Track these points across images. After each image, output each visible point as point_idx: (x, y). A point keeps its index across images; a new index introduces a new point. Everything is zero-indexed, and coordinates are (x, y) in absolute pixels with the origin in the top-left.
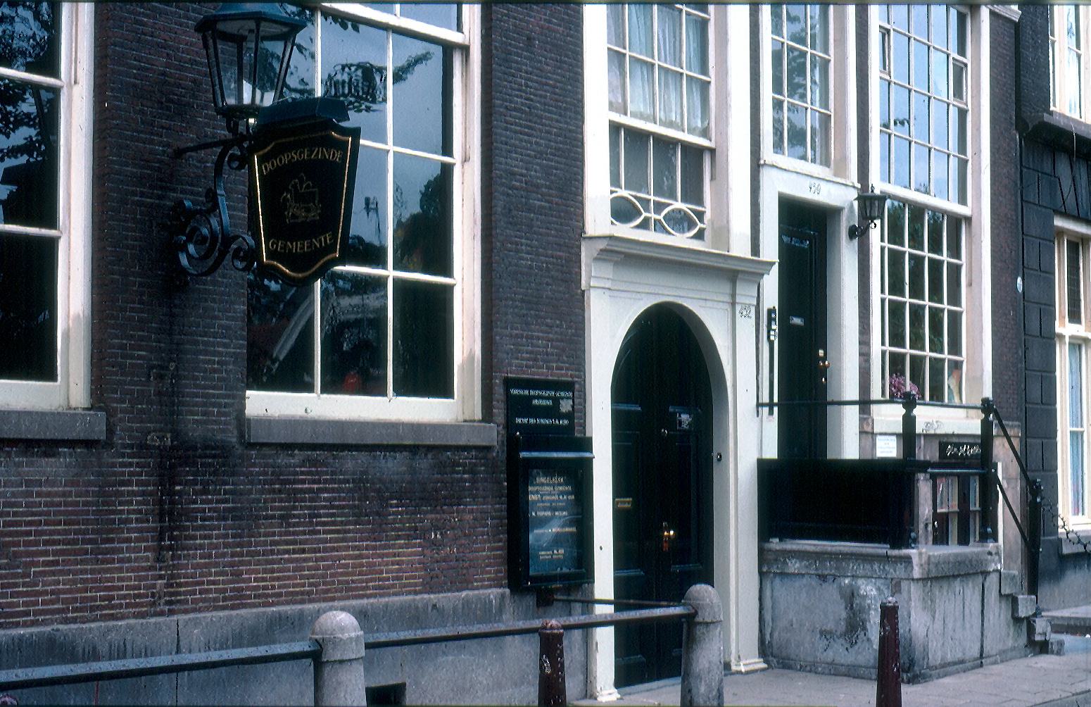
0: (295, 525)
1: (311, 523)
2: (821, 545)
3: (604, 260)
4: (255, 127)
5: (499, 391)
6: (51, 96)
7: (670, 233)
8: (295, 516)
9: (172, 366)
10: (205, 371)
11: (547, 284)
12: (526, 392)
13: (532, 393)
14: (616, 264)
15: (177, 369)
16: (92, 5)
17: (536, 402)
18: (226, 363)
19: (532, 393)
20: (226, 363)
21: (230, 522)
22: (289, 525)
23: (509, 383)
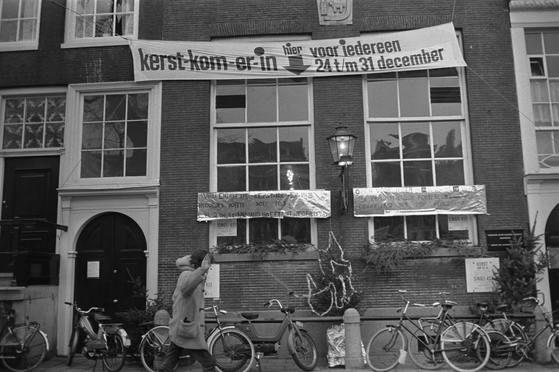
0: (390, 283)
1: (397, 283)
2: (36, 28)
3: (529, 183)
4: (135, 353)
5: (484, 237)
6: (459, 154)
7: (548, 167)
8: (390, 280)
9: (341, 237)
10: (353, 238)
11: (506, 195)
12: (496, 235)
13: (499, 235)
14: (541, 183)
15: (343, 238)
16: (36, 48)
17: (501, 238)
18: (361, 235)
19: (499, 235)
20: (361, 235)
21: (365, 282)
22: (388, 283)
23: (487, 232)
